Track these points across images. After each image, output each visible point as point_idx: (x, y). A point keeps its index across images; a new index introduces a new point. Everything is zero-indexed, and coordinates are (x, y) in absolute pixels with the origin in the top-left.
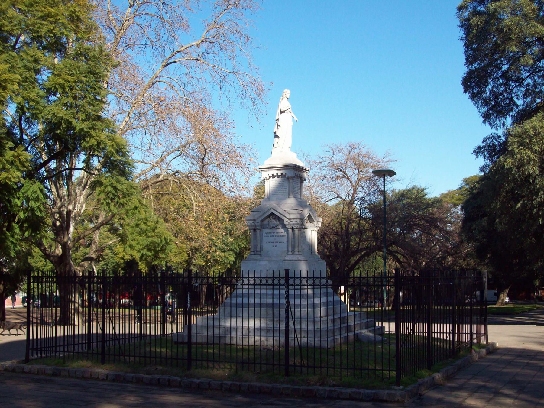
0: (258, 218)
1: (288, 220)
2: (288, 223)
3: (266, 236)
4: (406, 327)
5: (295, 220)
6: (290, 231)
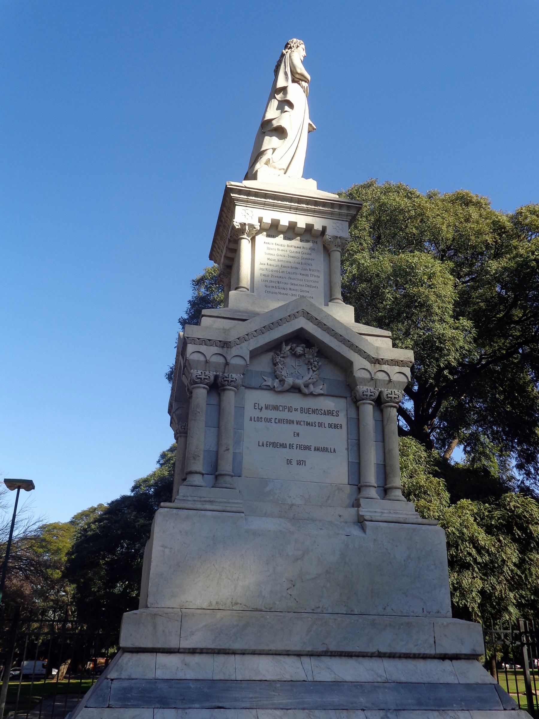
0: (241, 340)
1: (367, 364)
2: (367, 376)
3: (259, 419)
4: (71, 681)
5: (397, 369)
6: (368, 409)
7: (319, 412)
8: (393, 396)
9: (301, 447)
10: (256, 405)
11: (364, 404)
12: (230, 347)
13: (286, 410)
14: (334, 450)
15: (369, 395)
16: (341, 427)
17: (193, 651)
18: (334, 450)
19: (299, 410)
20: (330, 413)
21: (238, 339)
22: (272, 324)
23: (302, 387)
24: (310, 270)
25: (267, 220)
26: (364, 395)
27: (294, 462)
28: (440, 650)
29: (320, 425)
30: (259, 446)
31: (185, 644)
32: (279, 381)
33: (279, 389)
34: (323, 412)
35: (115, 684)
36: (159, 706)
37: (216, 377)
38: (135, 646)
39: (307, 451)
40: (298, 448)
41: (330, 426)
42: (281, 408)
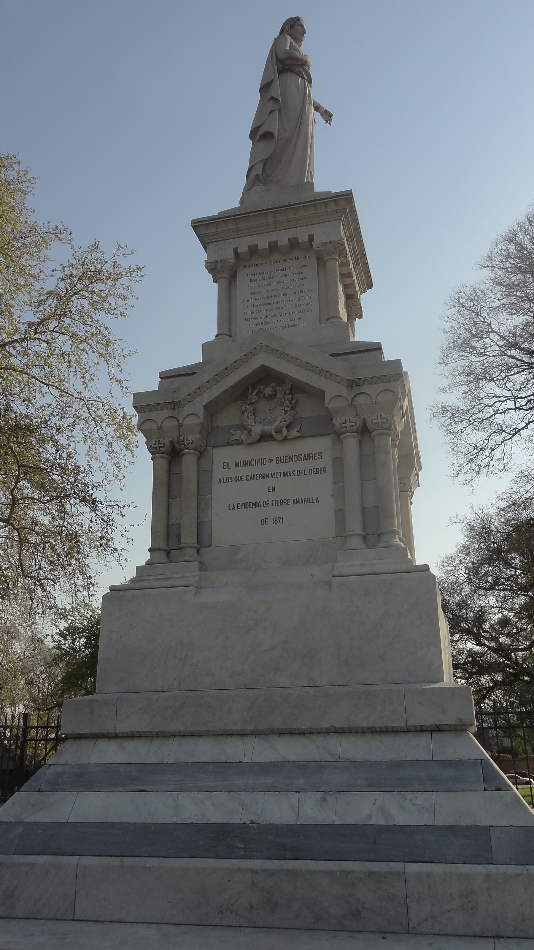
3: (229, 480)
7: (298, 458)
8: (380, 420)
9: (277, 503)
10: (225, 464)
11: (380, 434)
12: (181, 406)
13: (259, 464)
14: (317, 499)
15: (348, 427)
16: (325, 471)
17: (132, 736)
18: (317, 499)
19: (274, 461)
20: (311, 456)
21: (189, 395)
22: (226, 369)
23: (274, 433)
24: (302, 292)
25: (243, 249)
26: (342, 428)
27: (270, 521)
28: (413, 722)
29: (299, 473)
30: (229, 509)
31: (122, 728)
32: (248, 432)
33: (248, 442)
34: (302, 457)
35: (52, 770)
36: (84, 790)
37: (172, 442)
38: (74, 732)
39: (285, 506)
40: (274, 504)
41: (311, 472)
42: (253, 463)
